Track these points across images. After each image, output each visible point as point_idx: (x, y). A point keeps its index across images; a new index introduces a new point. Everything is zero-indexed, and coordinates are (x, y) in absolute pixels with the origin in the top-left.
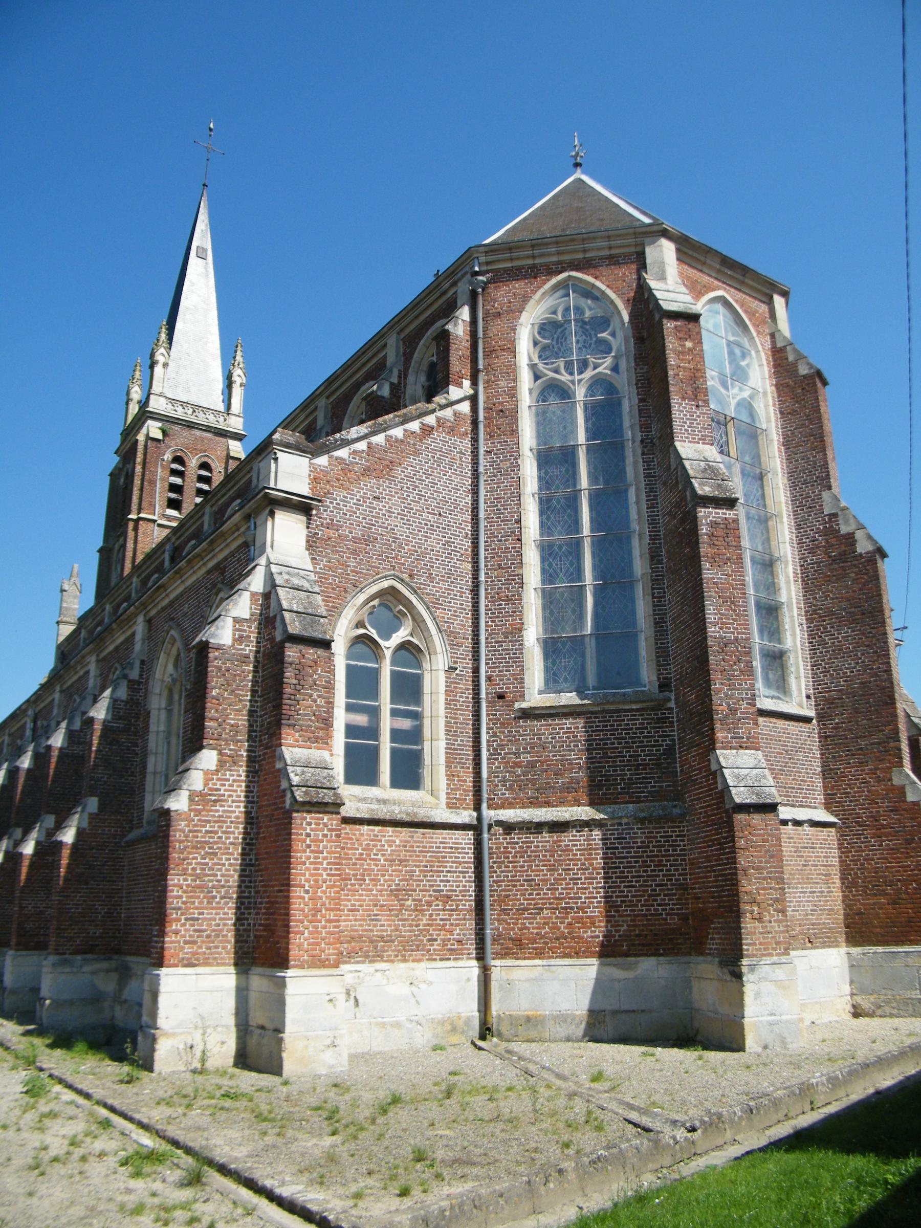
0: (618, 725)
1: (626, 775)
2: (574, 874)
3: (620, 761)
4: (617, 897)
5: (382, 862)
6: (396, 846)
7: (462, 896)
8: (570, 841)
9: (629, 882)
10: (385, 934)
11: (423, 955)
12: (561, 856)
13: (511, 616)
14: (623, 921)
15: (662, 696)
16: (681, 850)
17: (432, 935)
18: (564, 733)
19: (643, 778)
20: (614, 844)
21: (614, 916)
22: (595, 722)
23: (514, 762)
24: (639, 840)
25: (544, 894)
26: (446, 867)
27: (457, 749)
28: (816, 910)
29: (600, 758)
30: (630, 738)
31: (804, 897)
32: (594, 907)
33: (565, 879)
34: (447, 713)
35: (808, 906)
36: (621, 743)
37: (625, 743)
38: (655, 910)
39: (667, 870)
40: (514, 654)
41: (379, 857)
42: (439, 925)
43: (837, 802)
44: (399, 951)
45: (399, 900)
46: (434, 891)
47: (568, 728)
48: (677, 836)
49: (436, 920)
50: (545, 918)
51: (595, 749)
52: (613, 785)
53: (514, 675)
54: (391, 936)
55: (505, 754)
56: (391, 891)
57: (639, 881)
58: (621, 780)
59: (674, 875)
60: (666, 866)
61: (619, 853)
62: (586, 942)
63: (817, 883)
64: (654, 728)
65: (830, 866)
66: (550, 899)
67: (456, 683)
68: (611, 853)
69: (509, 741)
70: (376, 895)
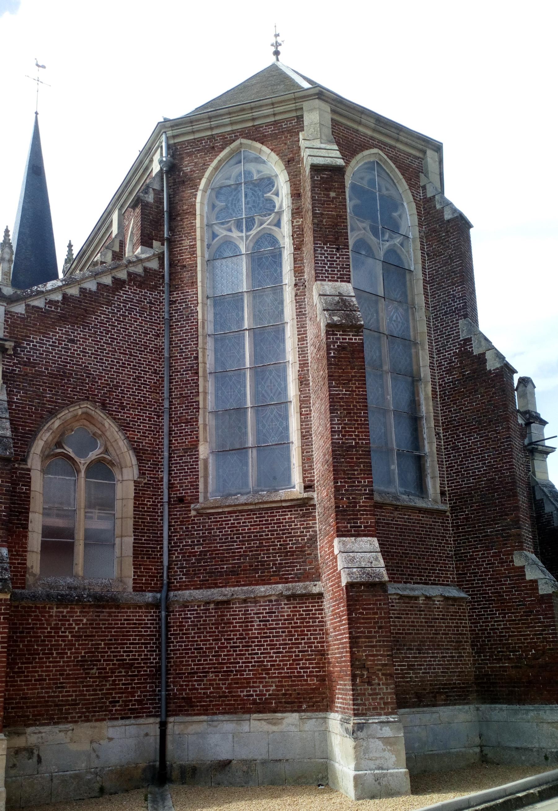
0: (271, 520)
1: (277, 560)
2: (234, 643)
3: (273, 549)
4: (268, 661)
5: (70, 638)
6: (83, 624)
7: (144, 663)
8: (231, 615)
9: (277, 648)
10: (70, 698)
11: (105, 715)
12: (224, 628)
13: (189, 435)
14: (272, 682)
15: (305, 495)
16: (319, 622)
17: (115, 697)
18: (228, 528)
19: (291, 563)
20: (266, 617)
21: (265, 678)
22: (253, 518)
23: (190, 553)
24: (286, 614)
25: (210, 660)
26: (130, 640)
27: (144, 544)
28: (447, 673)
29: (257, 547)
30: (280, 530)
31: (435, 661)
32: (249, 670)
33: (227, 647)
34: (134, 514)
35: (439, 669)
36: (273, 535)
37: (277, 534)
38: (298, 672)
39: (308, 639)
40: (191, 465)
41: (67, 634)
42: (121, 688)
43: (467, 581)
44: (83, 713)
45: (84, 669)
46: (117, 660)
47: (232, 524)
48: (316, 610)
49: (119, 684)
50: (210, 680)
51: (253, 540)
52: (267, 569)
53: (191, 482)
54: (76, 700)
55: (183, 546)
56: (77, 661)
57: (286, 648)
58: (273, 565)
59: (314, 643)
60: (307, 635)
61: (270, 625)
62: (244, 700)
63: (448, 649)
64: (301, 521)
65: (460, 634)
66: (214, 664)
67: (144, 490)
68: (263, 625)
69: (186, 535)
70: (63, 666)
